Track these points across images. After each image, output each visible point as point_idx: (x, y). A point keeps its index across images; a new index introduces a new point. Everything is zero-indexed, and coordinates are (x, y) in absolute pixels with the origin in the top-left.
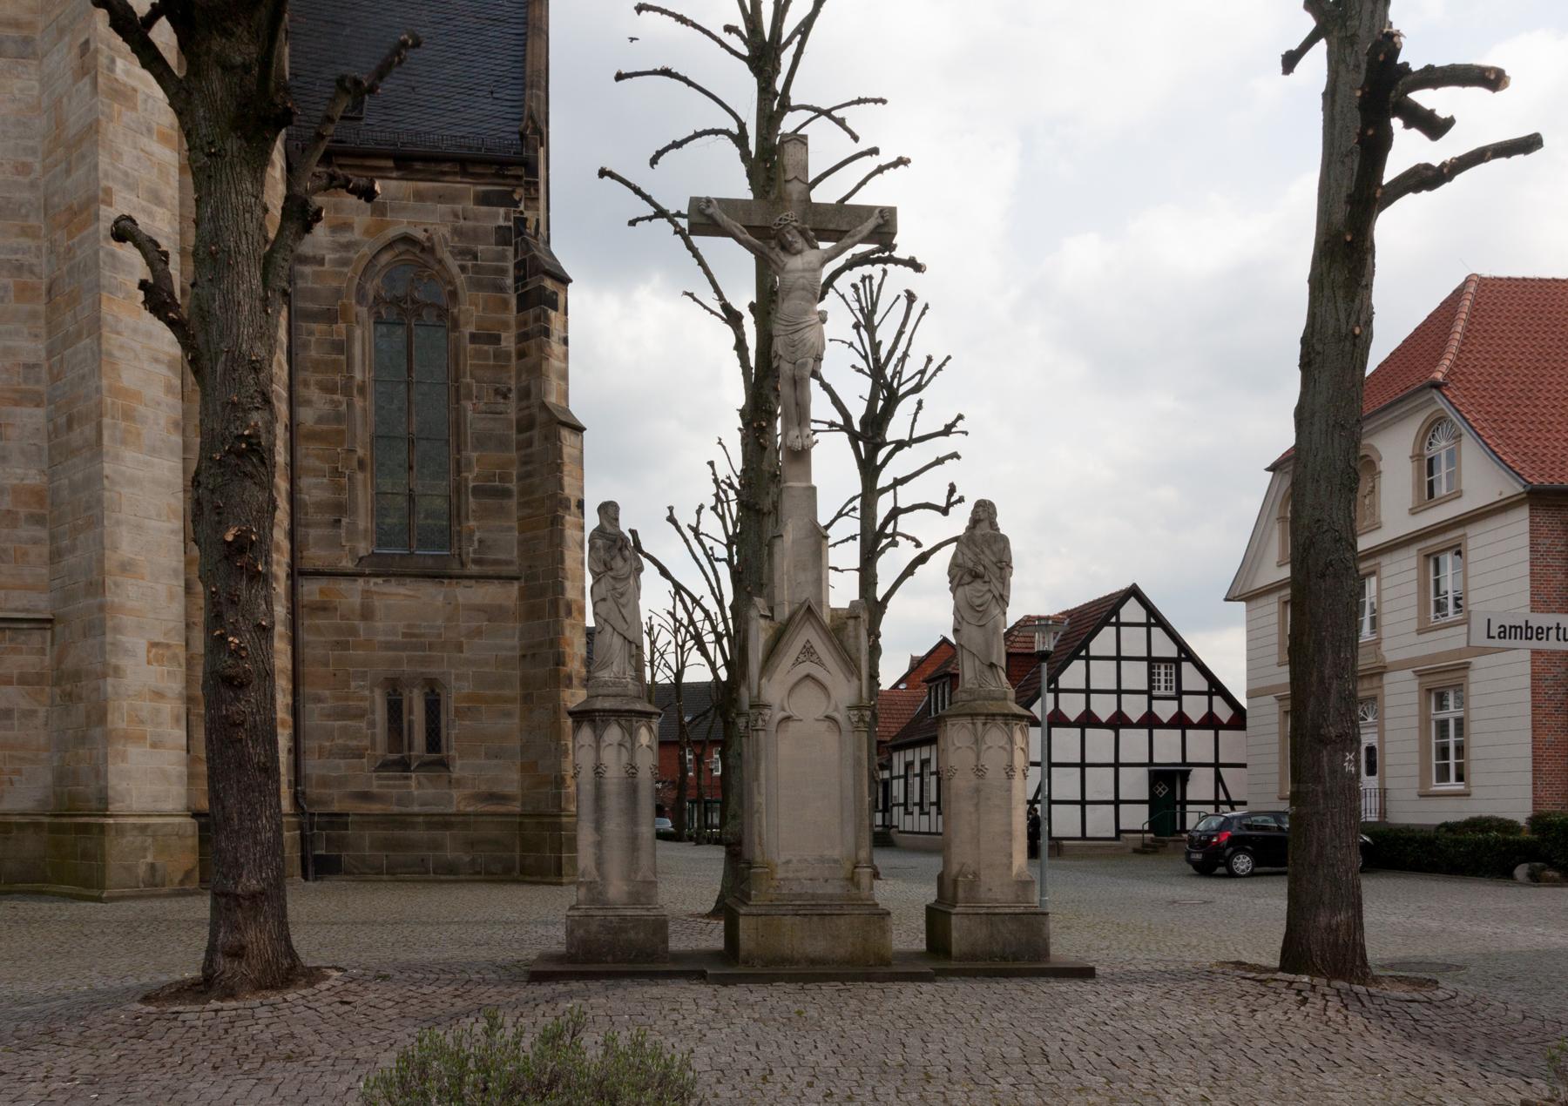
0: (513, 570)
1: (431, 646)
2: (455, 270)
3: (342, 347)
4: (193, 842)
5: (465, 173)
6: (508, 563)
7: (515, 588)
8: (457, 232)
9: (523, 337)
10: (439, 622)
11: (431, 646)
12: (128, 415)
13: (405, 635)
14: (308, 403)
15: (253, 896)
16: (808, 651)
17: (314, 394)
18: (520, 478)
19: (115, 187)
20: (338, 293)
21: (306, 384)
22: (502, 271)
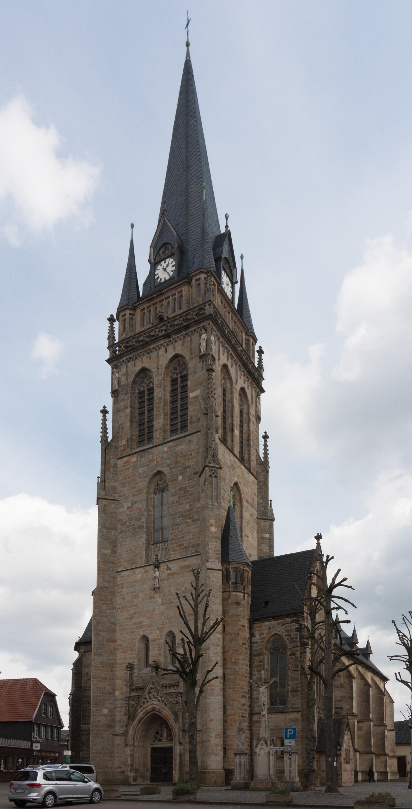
0: (300, 709)
1: (281, 729)
2: (286, 639)
3: (262, 661)
4: (224, 775)
5: (287, 617)
6: (298, 708)
7: (300, 714)
8: (286, 631)
9: (301, 653)
10: (283, 723)
11: (281, 729)
12: (212, 690)
13: (275, 727)
14: (255, 675)
15: (193, 778)
16: (262, 744)
17: (256, 673)
18: (301, 687)
19: (210, 646)
20: (261, 649)
21: (254, 671)
22: (297, 638)
